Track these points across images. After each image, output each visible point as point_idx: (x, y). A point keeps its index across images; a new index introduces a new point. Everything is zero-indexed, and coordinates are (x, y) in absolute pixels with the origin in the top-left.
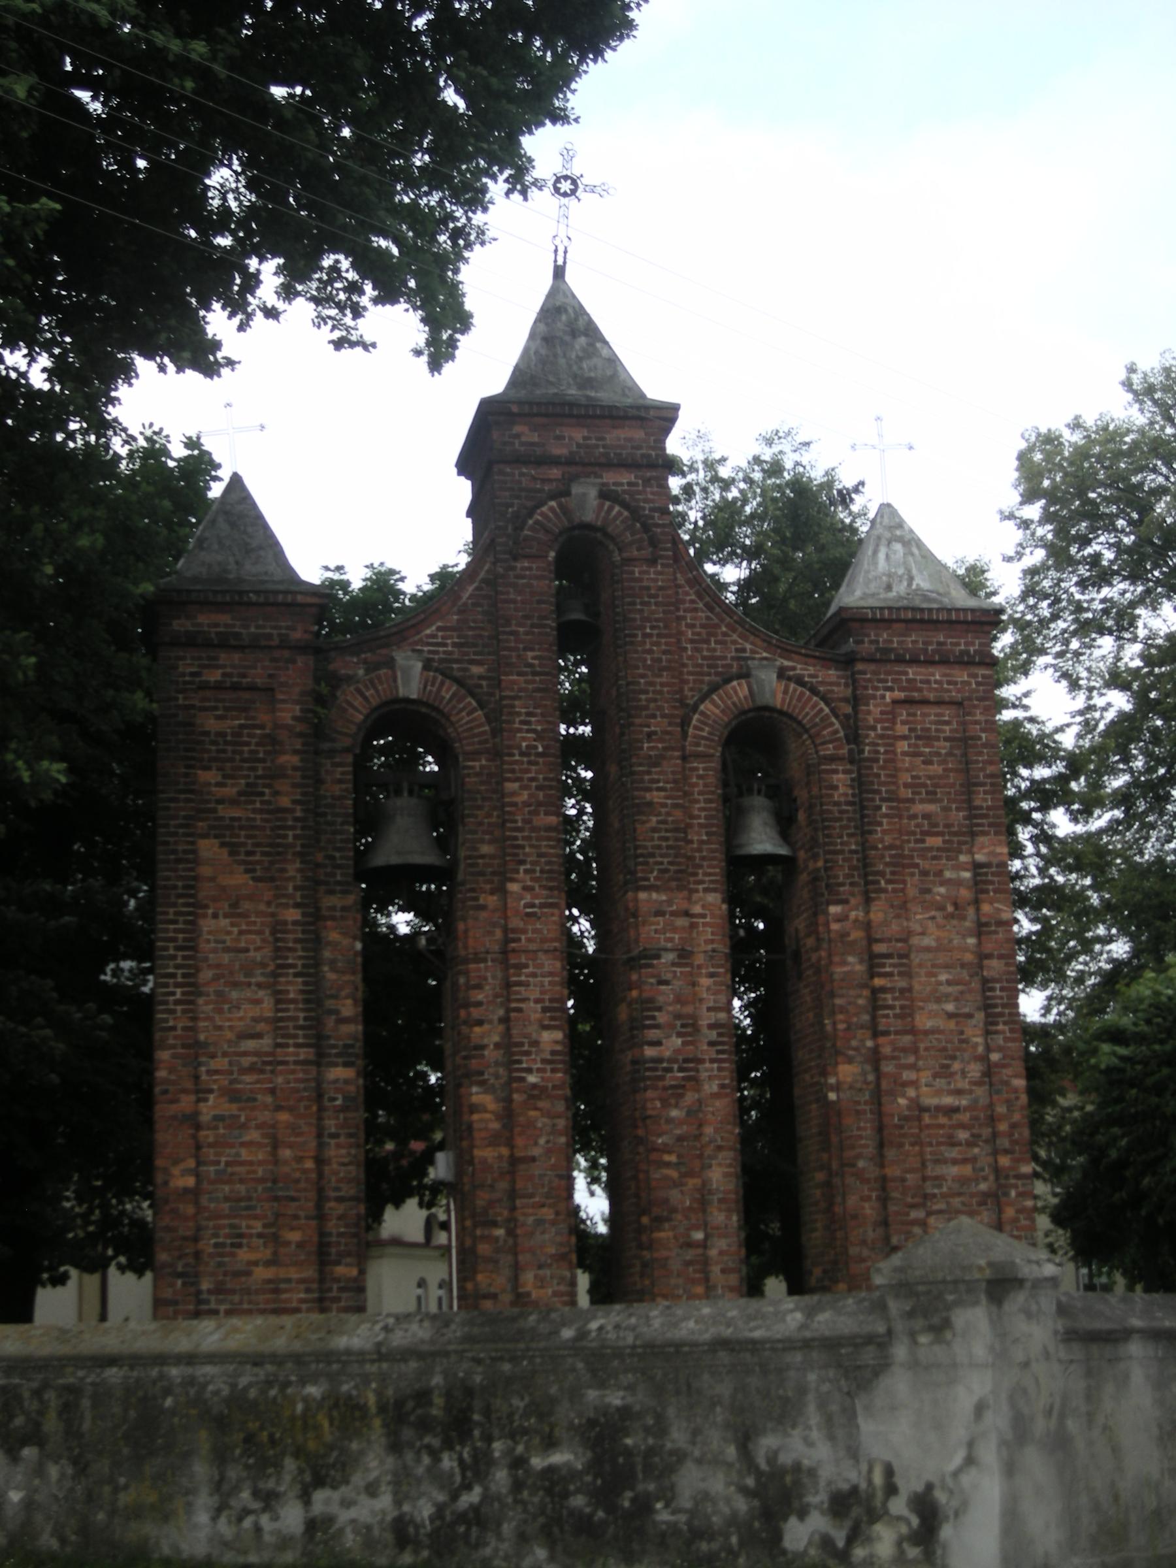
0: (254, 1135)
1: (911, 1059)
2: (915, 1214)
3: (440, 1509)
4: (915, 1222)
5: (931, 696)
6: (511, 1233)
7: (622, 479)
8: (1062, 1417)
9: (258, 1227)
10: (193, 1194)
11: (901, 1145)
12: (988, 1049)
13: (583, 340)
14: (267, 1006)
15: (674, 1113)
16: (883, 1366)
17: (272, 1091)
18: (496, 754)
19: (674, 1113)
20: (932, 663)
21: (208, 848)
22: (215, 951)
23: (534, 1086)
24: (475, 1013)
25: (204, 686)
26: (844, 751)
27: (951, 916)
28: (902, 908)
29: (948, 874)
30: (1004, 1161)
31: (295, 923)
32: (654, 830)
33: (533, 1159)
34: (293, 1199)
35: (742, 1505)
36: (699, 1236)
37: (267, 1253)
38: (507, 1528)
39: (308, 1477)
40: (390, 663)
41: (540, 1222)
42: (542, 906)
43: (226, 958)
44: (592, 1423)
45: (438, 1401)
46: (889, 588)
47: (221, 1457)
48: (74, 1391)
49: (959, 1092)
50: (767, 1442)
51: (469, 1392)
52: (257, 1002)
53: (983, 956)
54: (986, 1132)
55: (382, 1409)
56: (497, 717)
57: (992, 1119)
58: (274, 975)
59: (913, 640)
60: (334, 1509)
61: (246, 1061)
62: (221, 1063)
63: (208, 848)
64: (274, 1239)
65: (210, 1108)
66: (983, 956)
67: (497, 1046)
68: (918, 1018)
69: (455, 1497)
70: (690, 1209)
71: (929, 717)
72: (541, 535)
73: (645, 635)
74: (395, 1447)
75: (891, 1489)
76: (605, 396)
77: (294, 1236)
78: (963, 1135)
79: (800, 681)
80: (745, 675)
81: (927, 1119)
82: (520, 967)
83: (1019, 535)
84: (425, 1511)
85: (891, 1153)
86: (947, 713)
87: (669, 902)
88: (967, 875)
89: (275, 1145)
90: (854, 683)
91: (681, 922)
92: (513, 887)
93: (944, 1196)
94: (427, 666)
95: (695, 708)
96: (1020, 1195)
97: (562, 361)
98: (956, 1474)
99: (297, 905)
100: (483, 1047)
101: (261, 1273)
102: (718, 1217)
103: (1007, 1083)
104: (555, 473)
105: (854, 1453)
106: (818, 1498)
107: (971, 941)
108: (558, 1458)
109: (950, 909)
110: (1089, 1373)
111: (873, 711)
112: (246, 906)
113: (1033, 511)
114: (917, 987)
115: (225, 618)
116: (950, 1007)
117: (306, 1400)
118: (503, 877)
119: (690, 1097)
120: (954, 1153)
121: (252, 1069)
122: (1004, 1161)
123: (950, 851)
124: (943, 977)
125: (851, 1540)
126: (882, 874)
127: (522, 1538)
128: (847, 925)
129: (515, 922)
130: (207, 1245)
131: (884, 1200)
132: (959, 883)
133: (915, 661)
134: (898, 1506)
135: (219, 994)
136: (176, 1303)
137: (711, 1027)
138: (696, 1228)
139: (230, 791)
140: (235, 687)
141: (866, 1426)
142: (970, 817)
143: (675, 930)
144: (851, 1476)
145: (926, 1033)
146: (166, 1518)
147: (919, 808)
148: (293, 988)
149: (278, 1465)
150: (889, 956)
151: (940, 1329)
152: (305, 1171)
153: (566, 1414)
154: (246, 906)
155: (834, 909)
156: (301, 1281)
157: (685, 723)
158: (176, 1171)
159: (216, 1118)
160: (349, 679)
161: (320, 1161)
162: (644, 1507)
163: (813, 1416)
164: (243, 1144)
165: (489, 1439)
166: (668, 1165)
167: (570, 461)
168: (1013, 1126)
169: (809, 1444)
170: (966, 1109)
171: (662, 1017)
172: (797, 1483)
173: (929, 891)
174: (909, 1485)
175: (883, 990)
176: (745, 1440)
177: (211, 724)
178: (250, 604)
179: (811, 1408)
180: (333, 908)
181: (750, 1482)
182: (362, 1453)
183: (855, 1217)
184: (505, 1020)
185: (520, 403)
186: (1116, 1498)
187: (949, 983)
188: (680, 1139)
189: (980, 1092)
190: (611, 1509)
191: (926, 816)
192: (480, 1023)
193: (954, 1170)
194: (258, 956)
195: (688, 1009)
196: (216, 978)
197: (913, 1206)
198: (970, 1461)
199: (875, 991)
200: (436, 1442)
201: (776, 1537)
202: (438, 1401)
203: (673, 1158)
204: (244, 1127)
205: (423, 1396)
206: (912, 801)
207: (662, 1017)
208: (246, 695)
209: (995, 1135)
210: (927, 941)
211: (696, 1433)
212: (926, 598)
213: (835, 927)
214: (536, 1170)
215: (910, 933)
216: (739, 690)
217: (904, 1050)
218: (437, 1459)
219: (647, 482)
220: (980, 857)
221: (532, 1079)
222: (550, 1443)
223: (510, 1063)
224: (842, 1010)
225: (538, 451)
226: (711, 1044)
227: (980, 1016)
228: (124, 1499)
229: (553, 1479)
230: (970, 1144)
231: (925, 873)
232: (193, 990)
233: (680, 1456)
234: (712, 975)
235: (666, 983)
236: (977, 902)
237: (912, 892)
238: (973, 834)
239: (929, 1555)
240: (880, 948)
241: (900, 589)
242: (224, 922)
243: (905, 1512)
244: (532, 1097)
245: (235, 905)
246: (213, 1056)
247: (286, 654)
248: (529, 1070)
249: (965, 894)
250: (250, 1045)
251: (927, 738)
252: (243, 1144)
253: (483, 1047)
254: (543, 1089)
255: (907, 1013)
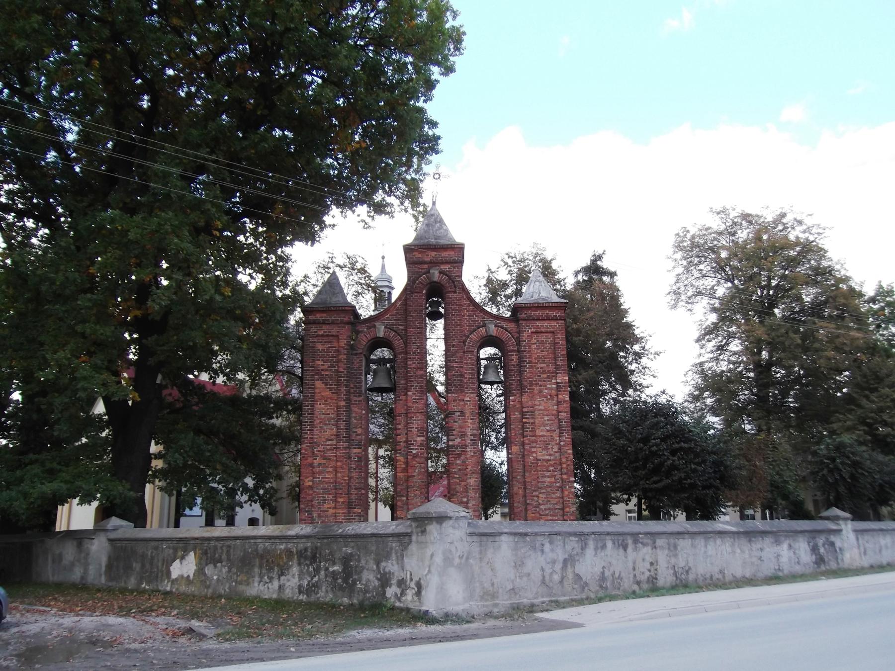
0: (330, 470)
1: (535, 445)
2: (537, 493)
3: (309, 582)
4: (534, 496)
5: (544, 330)
6: (407, 499)
7: (445, 267)
8: (467, 558)
9: (331, 497)
10: (311, 487)
11: (530, 472)
12: (560, 441)
13: (438, 225)
14: (334, 431)
15: (458, 462)
16: (410, 542)
17: (336, 456)
18: (406, 353)
19: (458, 462)
20: (544, 320)
21: (319, 384)
22: (320, 415)
23: (415, 454)
24: (398, 432)
25: (318, 336)
26: (516, 349)
27: (549, 399)
28: (532, 397)
29: (548, 386)
30: (565, 477)
31: (344, 406)
32: (454, 375)
33: (414, 476)
34: (341, 489)
35: (377, 583)
36: (465, 500)
37: (333, 505)
38: (324, 588)
39: (280, 573)
40: (375, 326)
41: (415, 495)
42: (418, 399)
43: (323, 416)
44: (344, 558)
45: (309, 550)
46: (532, 297)
47: (261, 567)
48: (229, 547)
49: (550, 455)
50: (383, 564)
51: (316, 548)
52: (332, 430)
53: (559, 412)
54: (559, 467)
55: (297, 553)
56: (406, 343)
57: (561, 464)
58: (337, 421)
59: (538, 313)
60: (285, 582)
61: (328, 447)
62: (321, 448)
63: (319, 384)
64: (336, 501)
65: (316, 462)
66: (559, 412)
67: (405, 442)
68: (537, 431)
69: (312, 579)
70: (463, 491)
71: (543, 337)
72: (420, 286)
73: (453, 315)
74: (299, 564)
75: (411, 580)
76: (443, 242)
77: (341, 500)
78: (551, 468)
79: (502, 327)
80: (485, 326)
81: (540, 463)
82: (411, 418)
83: (673, 264)
84: (305, 583)
85: (527, 474)
86: (549, 335)
87: (458, 397)
88: (555, 386)
89: (336, 471)
90: (518, 327)
91: (462, 403)
92: (410, 393)
93: (545, 487)
94: (385, 327)
95: (468, 337)
96: (569, 487)
97: (431, 231)
98: (426, 575)
99: (344, 400)
100: (401, 442)
101: (331, 511)
102: (472, 494)
103: (566, 452)
104: (426, 266)
105: (403, 568)
106: (394, 581)
107: (556, 407)
108: (336, 568)
109: (549, 397)
110: (481, 545)
111: (524, 336)
112: (329, 401)
113: (679, 255)
114: (536, 421)
115: (324, 315)
116: (548, 428)
117: (281, 549)
118: (407, 390)
119: (463, 457)
120: (548, 474)
121: (330, 450)
122: (565, 477)
123: (549, 379)
124: (546, 419)
125: (401, 594)
126: (526, 387)
127: (327, 591)
128: (516, 403)
129: (410, 404)
130: (315, 503)
131: (525, 488)
132: (551, 389)
133: (538, 320)
134: (413, 585)
135: (321, 427)
136: (305, 520)
137: (471, 435)
138: (464, 497)
139: (325, 367)
140: (327, 336)
141: (406, 560)
142: (555, 368)
143: (459, 405)
144: (403, 575)
145: (540, 436)
146: (248, 584)
147: (539, 365)
148: (342, 425)
149: (273, 569)
150: (527, 412)
151: (424, 532)
152: (345, 480)
153: (338, 555)
154: (329, 401)
155: (511, 398)
156: (343, 513)
157: (464, 342)
158: (306, 480)
159: (320, 465)
160: (362, 332)
161: (350, 478)
162: (354, 583)
163: (394, 556)
164: (327, 472)
165: (320, 562)
166: (456, 478)
167: (430, 263)
168: (568, 465)
169: (393, 565)
170: (553, 460)
171: (455, 432)
172: (390, 577)
173: (542, 392)
174: (415, 579)
175: (526, 423)
176: (378, 564)
177: (320, 346)
178: (331, 310)
179: (394, 555)
180: (355, 401)
181: (379, 576)
182: (292, 565)
183: (516, 494)
184: (407, 434)
185: (415, 246)
186: (493, 584)
187: (548, 420)
188: (460, 470)
189: (557, 455)
190: (347, 583)
191: (541, 368)
192: (400, 435)
193: (548, 479)
194: (333, 416)
195: (463, 430)
196: (320, 423)
197: (535, 491)
198: (429, 571)
199: (524, 423)
200: (308, 562)
201: (384, 593)
202: (309, 550)
203: (458, 476)
204: (327, 467)
205: (306, 549)
206: (537, 363)
207: (455, 432)
208: (331, 338)
209: (562, 468)
210: (542, 407)
211: (367, 561)
212: (543, 299)
213: (511, 403)
214: (415, 480)
215: (536, 405)
216: (482, 330)
217: (533, 442)
218: (309, 568)
219: (454, 267)
220: (558, 381)
221: (414, 452)
222: (334, 564)
223: (407, 447)
224: (514, 429)
225: (421, 260)
226: (471, 440)
227: (558, 431)
228: (239, 579)
229: (334, 575)
230: (554, 471)
231: (541, 386)
232: (312, 425)
233: (363, 568)
234: (472, 419)
235: (456, 422)
236: (557, 395)
237: (536, 392)
238: (557, 373)
239: (419, 599)
240: (525, 410)
241: (536, 297)
242: (323, 406)
243: (414, 587)
244: (414, 457)
245: (326, 401)
246: (319, 446)
247: (343, 325)
248: (413, 449)
249: (554, 392)
250: (330, 442)
251: (542, 343)
252: (327, 472)
253: (401, 442)
254: (418, 455)
255: (533, 430)
